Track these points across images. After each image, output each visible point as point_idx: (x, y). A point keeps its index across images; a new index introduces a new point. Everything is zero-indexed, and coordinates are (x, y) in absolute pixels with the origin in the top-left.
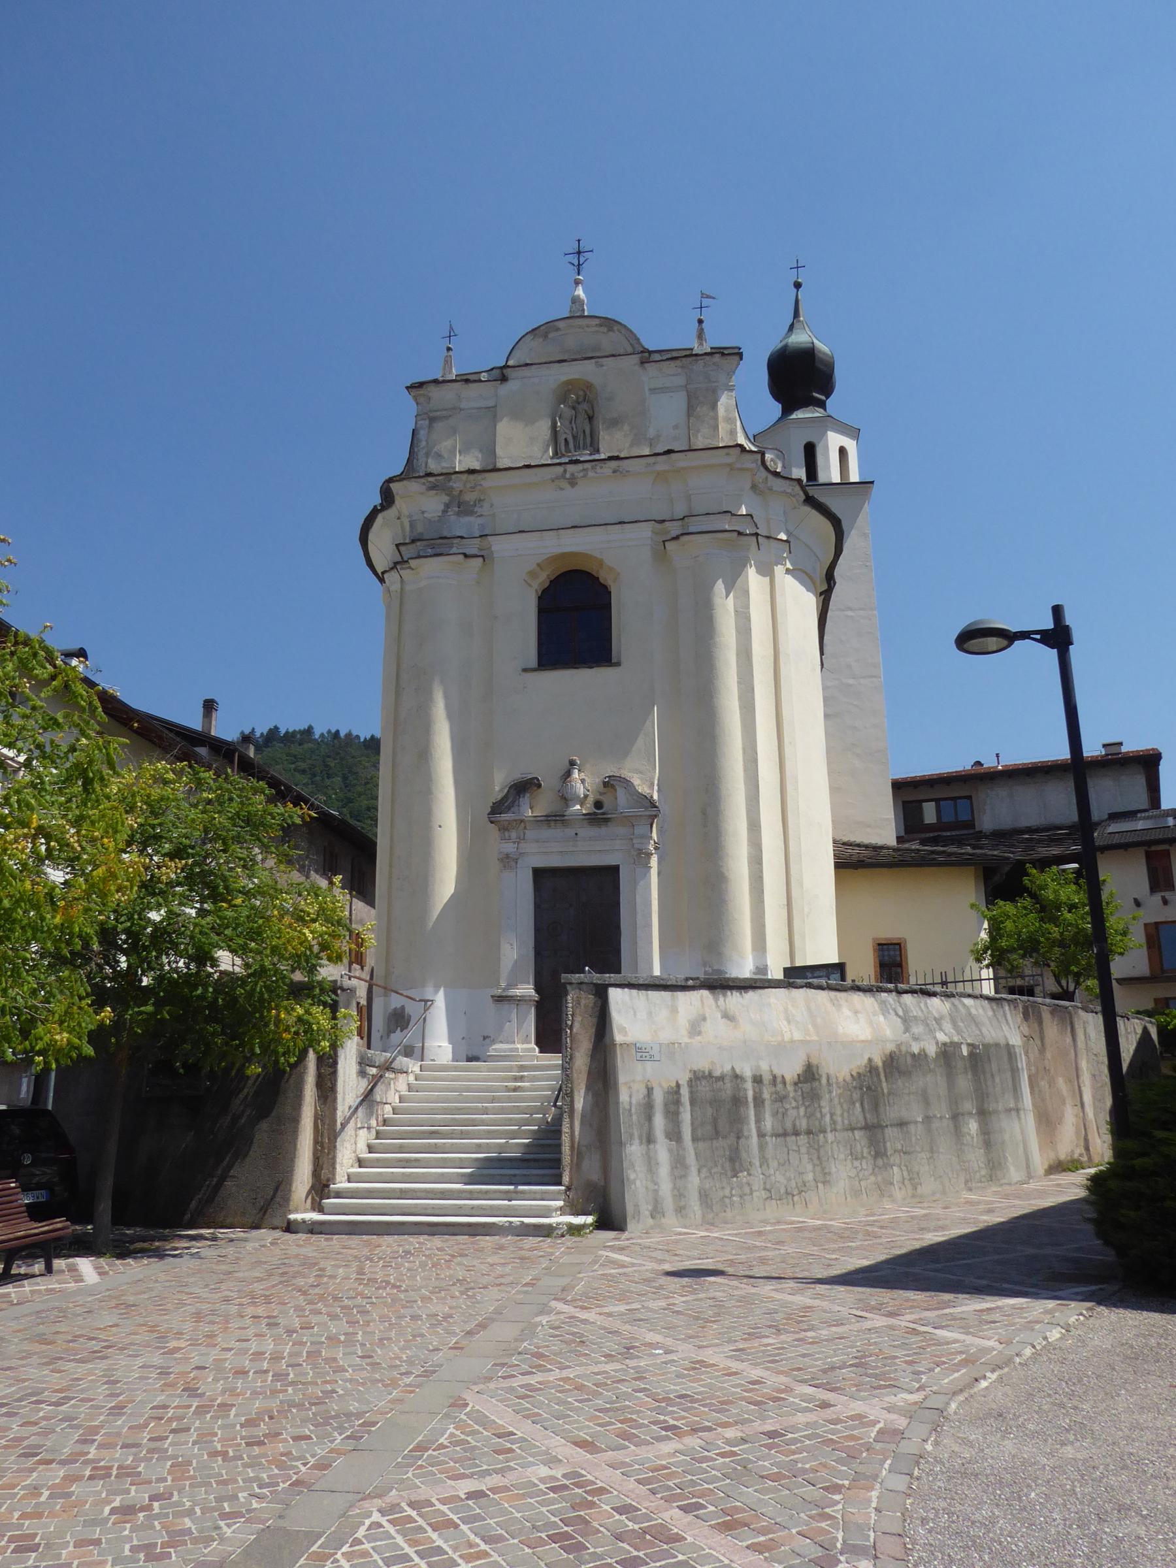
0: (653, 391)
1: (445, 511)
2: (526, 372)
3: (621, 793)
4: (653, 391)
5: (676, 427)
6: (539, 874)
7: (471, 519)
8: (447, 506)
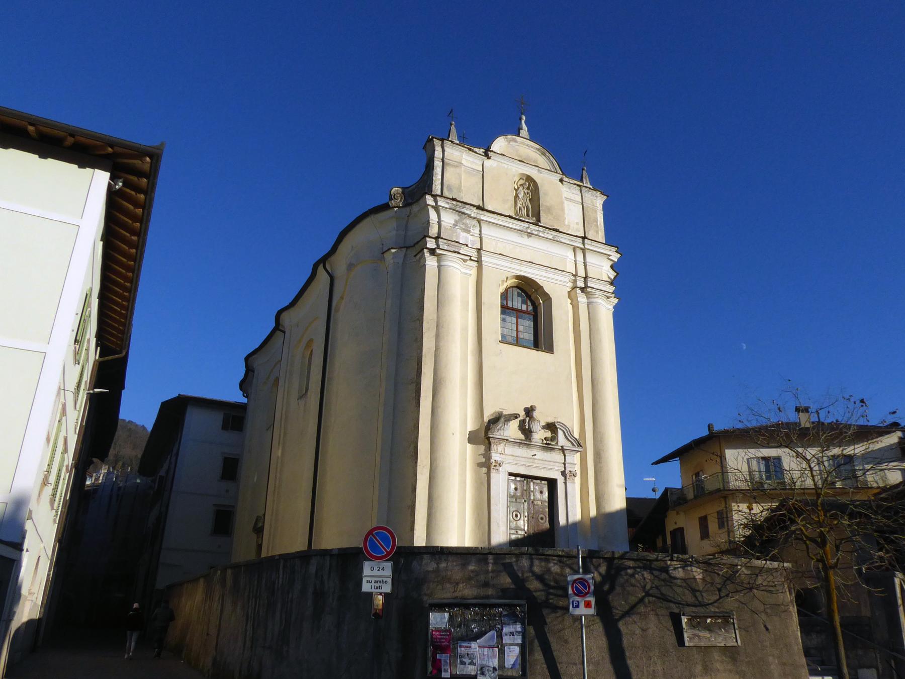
1: (455, 225)
2: (500, 158)
5: (577, 224)
7: (468, 235)
8: (456, 222)
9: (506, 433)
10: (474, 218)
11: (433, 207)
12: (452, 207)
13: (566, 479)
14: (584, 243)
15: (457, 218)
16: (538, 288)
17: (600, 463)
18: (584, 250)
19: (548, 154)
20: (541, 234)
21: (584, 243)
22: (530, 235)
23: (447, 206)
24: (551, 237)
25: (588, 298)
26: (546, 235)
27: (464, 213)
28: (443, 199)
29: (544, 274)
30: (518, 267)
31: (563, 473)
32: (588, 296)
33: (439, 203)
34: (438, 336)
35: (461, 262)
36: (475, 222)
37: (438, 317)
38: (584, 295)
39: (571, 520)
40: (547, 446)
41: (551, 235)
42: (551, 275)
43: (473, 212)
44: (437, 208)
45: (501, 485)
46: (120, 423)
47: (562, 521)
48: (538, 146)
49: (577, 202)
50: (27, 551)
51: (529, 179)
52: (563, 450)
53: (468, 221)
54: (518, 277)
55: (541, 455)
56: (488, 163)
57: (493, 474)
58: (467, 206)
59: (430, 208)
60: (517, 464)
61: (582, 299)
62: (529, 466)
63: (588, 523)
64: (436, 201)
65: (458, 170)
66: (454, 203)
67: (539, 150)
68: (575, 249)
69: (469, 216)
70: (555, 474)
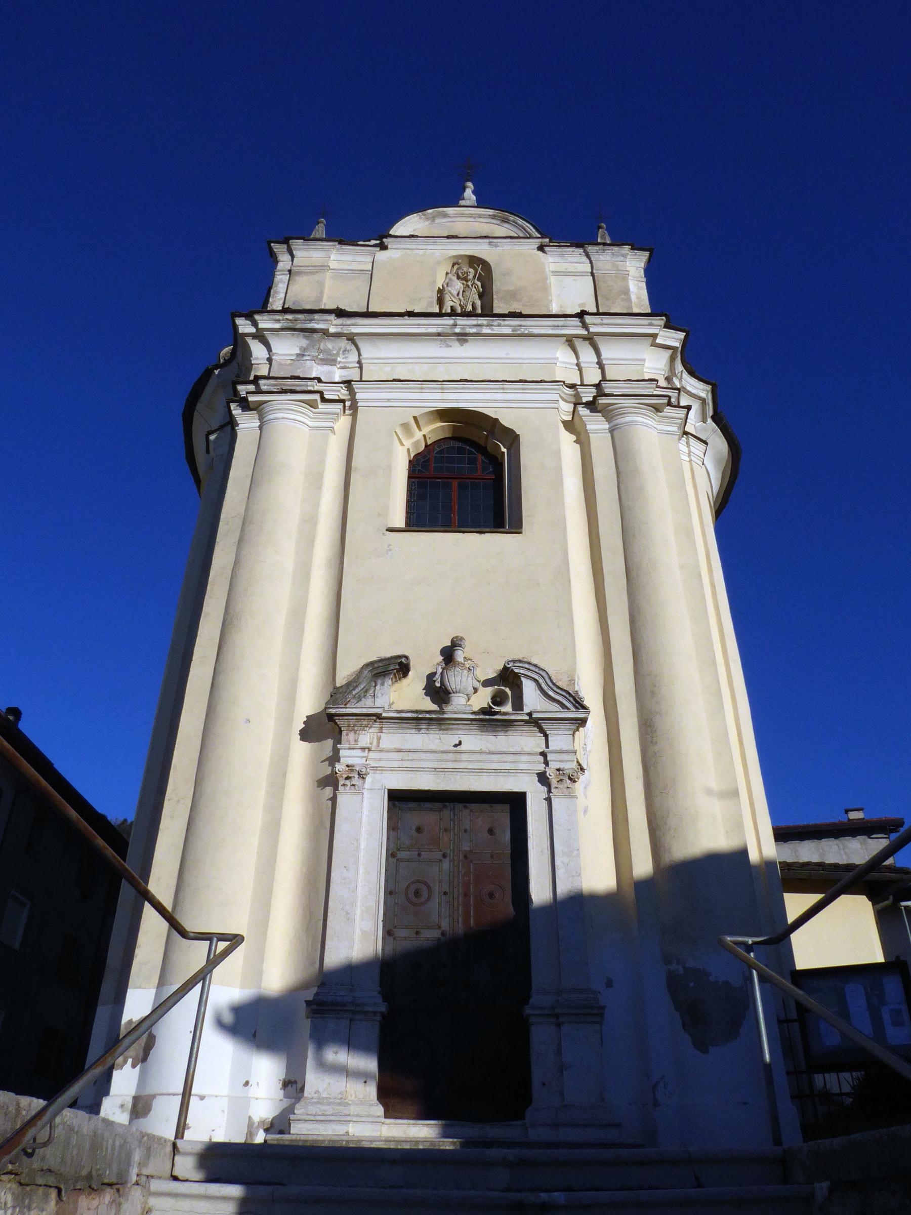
0: (556, 273)
2: (410, 244)
3: (529, 689)
4: (556, 273)
6: (398, 799)
9: (379, 702)
10: (338, 335)
11: (254, 336)
12: (286, 325)
13: (549, 791)
14: (585, 326)
15: (303, 342)
16: (491, 425)
17: (653, 743)
18: (590, 339)
19: (512, 218)
20: (485, 330)
21: (585, 326)
22: (463, 337)
23: (277, 326)
24: (508, 331)
25: (609, 419)
26: (497, 330)
27: (314, 331)
28: (266, 316)
29: (499, 396)
30: (438, 396)
31: (543, 778)
32: (608, 413)
33: (261, 325)
34: (241, 541)
35: (306, 409)
36: (343, 343)
37: (247, 510)
38: (598, 417)
39: (563, 889)
40: (488, 720)
41: (507, 326)
42: (514, 394)
43: (334, 325)
44: (260, 336)
45: (364, 823)
46: (407, 940)
47: (539, 892)
48: (491, 212)
49: (582, 274)
50: (223, 1111)
51: (474, 261)
52: (535, 723)
53: (329, 345)
54: (444, 414)
55: (474, 741)
56: (381, 255)
57: (345, 799)
58: (317, 316)
59: (249, 340)
60: (412, 770)
61: (596, 425)
62: (444, 770)
63: (630, 893)
64: (255, 324)
65: (317, 277)
66: (290, 317)
67: (493, 217)
68: (570, 341)
69: (325, 332)
70: (522, 782)
